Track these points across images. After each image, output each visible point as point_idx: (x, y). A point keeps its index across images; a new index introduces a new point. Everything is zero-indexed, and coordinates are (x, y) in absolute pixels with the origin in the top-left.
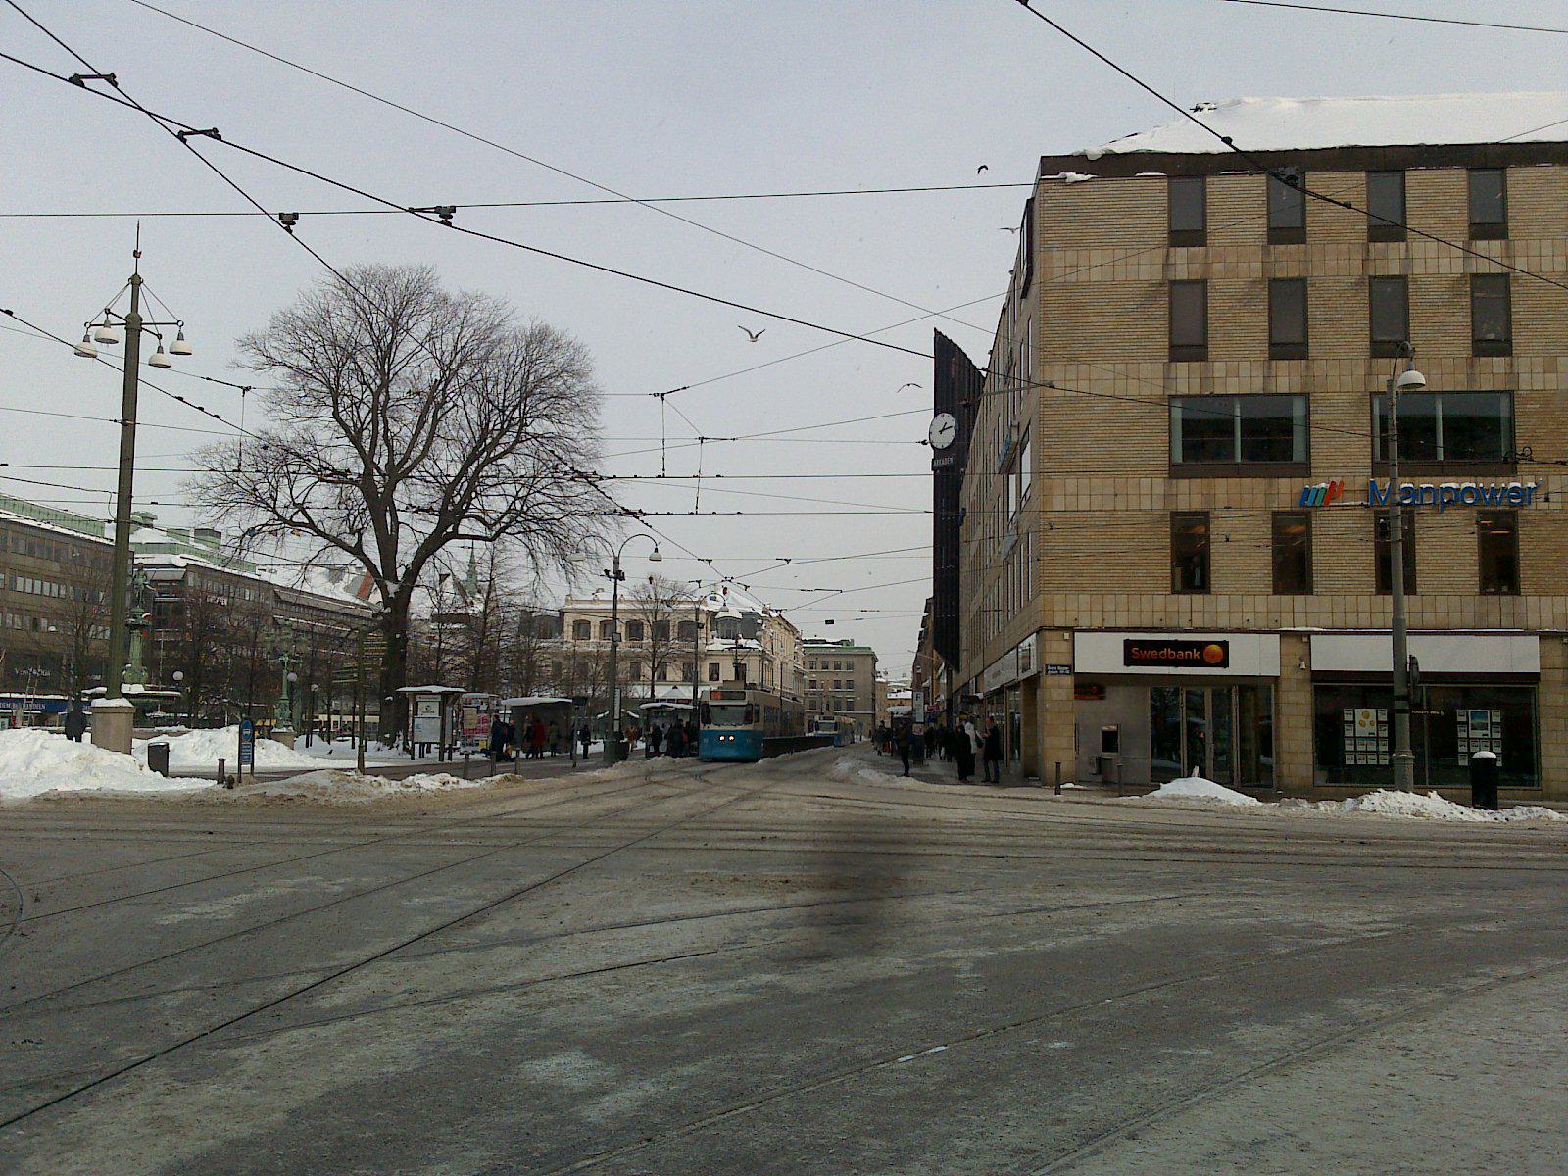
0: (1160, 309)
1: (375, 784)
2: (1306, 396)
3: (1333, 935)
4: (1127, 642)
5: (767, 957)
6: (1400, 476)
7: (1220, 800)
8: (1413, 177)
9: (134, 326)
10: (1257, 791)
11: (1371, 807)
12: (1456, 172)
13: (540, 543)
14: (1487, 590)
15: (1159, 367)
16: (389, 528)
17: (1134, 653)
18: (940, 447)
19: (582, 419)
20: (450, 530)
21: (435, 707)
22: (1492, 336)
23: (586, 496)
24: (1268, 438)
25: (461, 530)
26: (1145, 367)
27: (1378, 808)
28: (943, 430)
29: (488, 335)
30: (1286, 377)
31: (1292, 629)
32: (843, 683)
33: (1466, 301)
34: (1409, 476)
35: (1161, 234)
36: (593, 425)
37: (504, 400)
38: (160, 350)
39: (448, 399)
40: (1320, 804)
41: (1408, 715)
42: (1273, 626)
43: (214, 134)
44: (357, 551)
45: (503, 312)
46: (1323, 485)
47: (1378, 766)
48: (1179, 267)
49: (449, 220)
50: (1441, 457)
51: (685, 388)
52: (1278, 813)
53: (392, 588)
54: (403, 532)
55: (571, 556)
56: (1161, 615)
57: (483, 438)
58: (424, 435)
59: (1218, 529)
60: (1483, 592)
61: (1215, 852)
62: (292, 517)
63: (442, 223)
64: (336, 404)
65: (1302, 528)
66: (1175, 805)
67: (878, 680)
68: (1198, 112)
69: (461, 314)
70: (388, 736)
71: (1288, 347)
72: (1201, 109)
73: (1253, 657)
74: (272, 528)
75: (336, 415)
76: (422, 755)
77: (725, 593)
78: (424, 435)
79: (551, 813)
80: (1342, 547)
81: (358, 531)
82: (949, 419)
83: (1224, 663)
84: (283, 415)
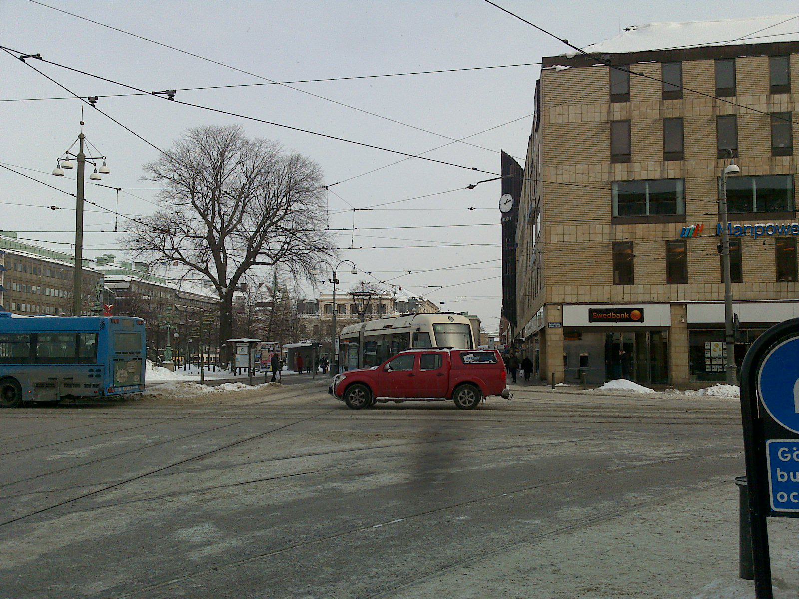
0: (606, 137)
1: (199, 388)
2: (683, 179)
3: (647, 460)
4: (590, 310)
5: (340, 474)
6: (728, 221)
7: (634, 391)
8: (739, 61)
9: (81, 160)
10: (654, 386)
11: (712, 393)
12: (762, 58)
13: (298, 267)
14: (781, 279)
15: (605, 167)
16: (222, 260)
17: (594, 315)
18: (505, 212)
19: (317, 202)
20: (252, 260)
21: (246, 350)
22: (782, 145)
23: (320, 241)
24: (663, 203)
25: (257, 260)
26: (598, 167)
27: (716, 394)
28: (507, 202)
29: (270, 162)
30: (673, 170)
31: (677, 302)
33: (768, 127)
34: (738, 220)
35: (605, 95)
36: (322, 204)
37: (278, 193)
38: (95, 171)
39: (250, 193)
40: (685, 392)
41: (733, 345)
42: (666, 300)
43: (38, 57)
44: (206, 271)
45: (277, 148)
46: (692, 226)
47: (711, 372)
48: (615, 114)
49: (173, 98)
50: (755, 210)
51: (337, 183)
52: (663, 397)
53: (224, 290)
54: (229, 261)
55: (313, 272)
56: (608, 296)
57: (268, 212)
58: (238, 214)
59: (638, 250)
60: (778, 279)
61: (623, 417)
62: (173, 254)
63: (169, 99)
64: (193, 197)
65: (682, 249)
66: (612, 394)
67: (481, 332)
68: (627, 31)
69: (256, 149)
70: (223, 364)
71: (673, 154)
72: (629, 30)
73: (656, 316)
74: (163, 261)
75: (193, 203)
76: (240, 373)
77: (400, 290)
78: (238, 214)
79: (283, 402)
80: (703, 259)
81: (205, 261)
82: (509, 197)
83: (641, 320)
84: (167, 204)
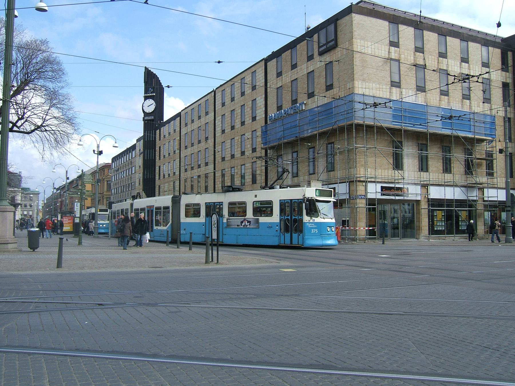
4: (382, 187)
32: (28, 205)
73: (413, 192)
